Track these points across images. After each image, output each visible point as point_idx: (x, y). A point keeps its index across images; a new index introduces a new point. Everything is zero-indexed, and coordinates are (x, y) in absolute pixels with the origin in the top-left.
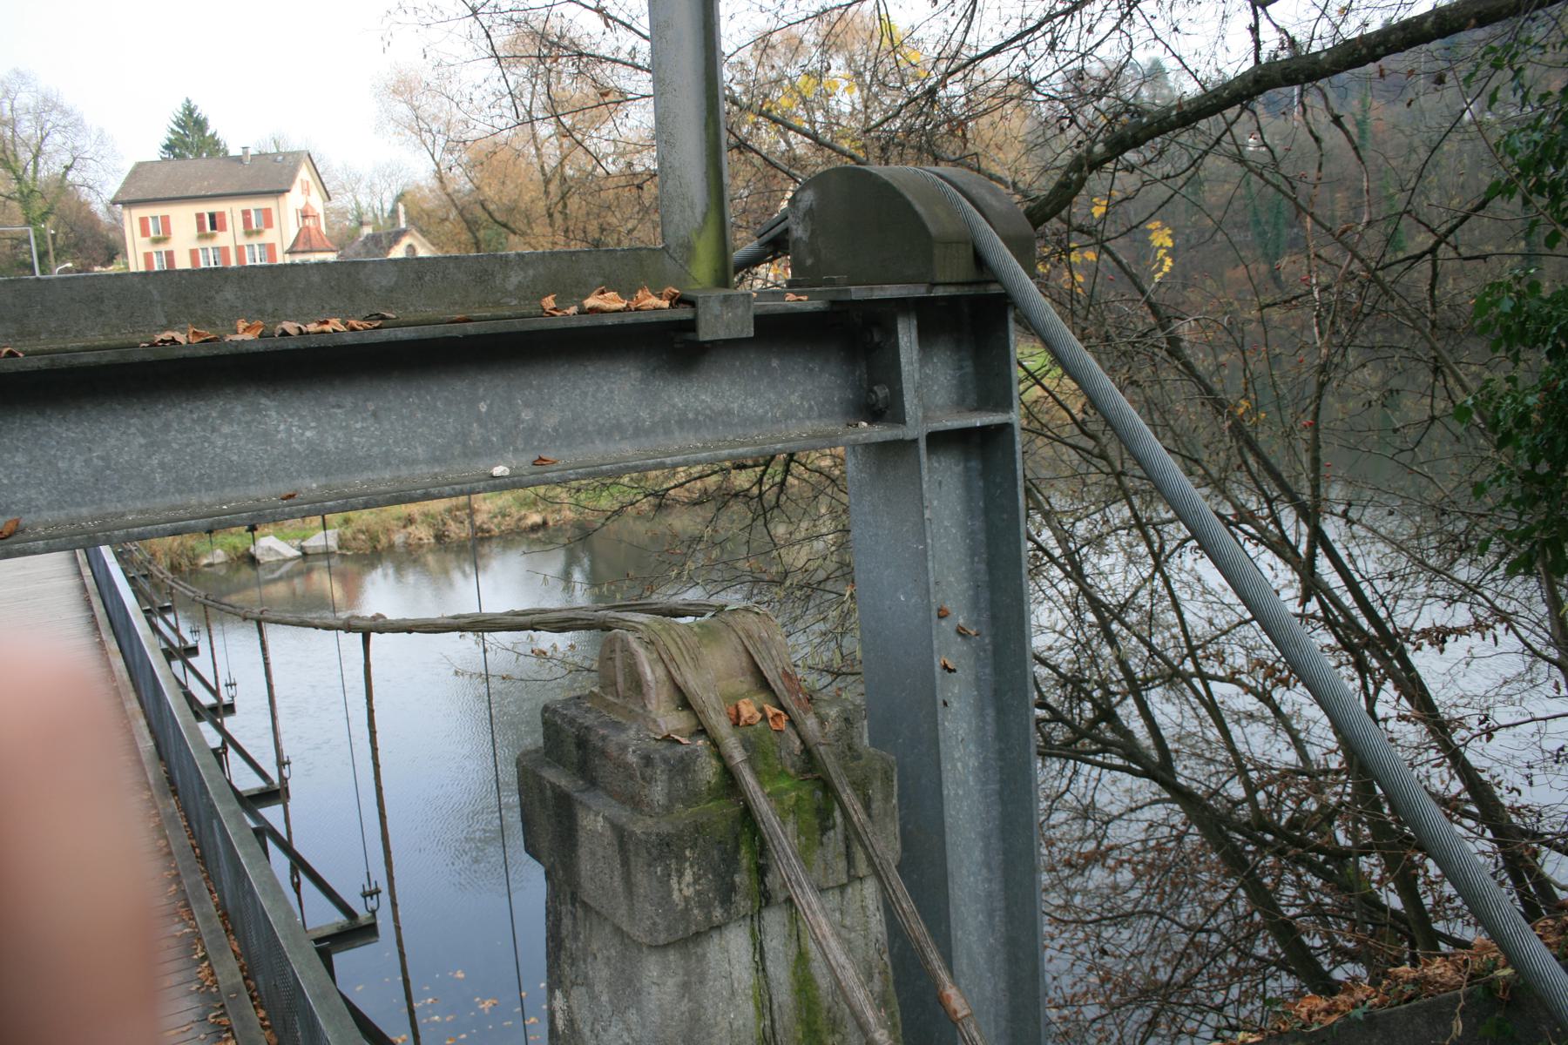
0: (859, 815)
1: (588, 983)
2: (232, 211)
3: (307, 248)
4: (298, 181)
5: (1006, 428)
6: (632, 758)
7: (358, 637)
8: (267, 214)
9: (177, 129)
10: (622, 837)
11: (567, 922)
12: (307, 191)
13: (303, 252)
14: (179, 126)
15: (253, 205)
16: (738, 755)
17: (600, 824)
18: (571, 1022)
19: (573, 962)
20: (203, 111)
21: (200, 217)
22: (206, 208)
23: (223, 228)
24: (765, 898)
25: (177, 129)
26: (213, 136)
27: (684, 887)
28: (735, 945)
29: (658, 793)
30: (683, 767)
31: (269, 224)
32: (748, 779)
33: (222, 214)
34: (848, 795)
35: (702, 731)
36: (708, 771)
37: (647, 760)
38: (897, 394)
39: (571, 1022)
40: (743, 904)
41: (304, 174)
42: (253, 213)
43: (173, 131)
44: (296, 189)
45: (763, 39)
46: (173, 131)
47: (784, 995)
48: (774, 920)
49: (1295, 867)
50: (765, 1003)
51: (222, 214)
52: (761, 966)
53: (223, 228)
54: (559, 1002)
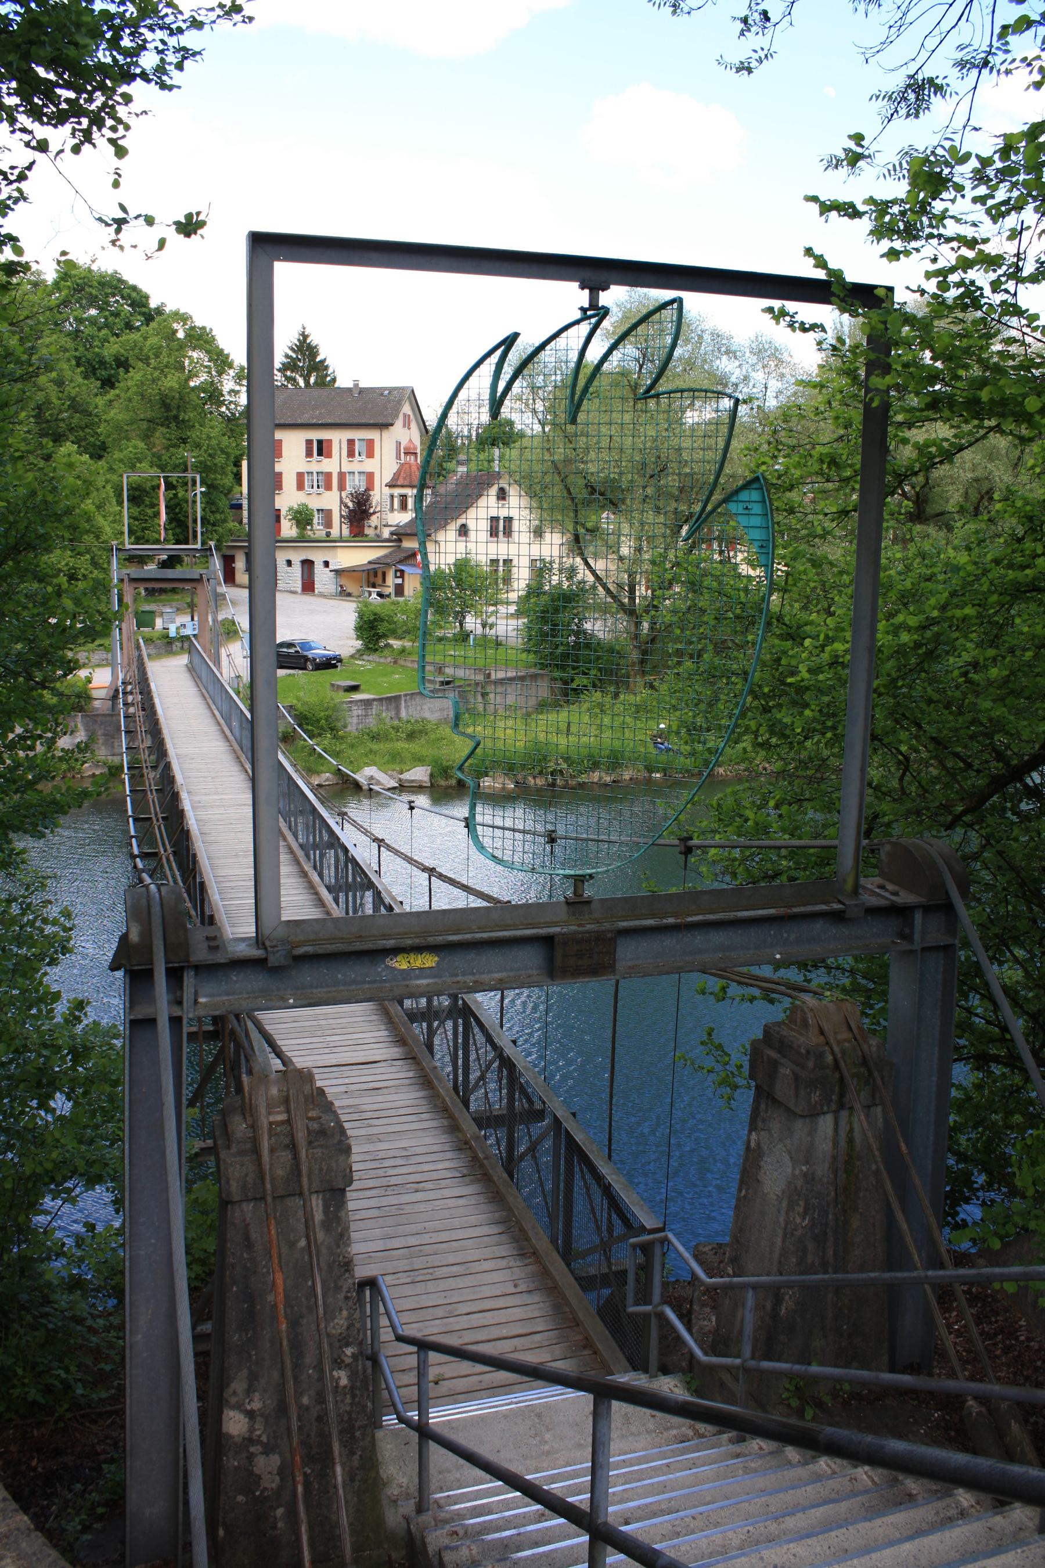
0: (879, 1082)
1: (769, 1130)
2: (338, 438)
3: (406, 483)
4: (401, 416)
5: (953, 945)
6: (803, 1051)
7: (426, 875)
8: (370, 443)
9: (291, 353)
10: (796, 1077)
11: (763, 1106)
12: (407, 424)
13: (402, 486)
14: (292, 349)
15: (357, 435)
16: (839, 1056)
17: (788, 1071)
18: (758, 1144)
19: (764, 1121)
20: (314, 339)
21: (309, 442)
22: (315, 435)
23: (329, 455)
24: (841, 1106)
25: (291, 353)
26: (323, 361)
27: (815, 1097)
28: (826, 1123)
29: (811, 1064)
30: (820, 1056)
31: (370, 454)
32: (842, 1064)
33: (330, 441)
34: (876, 1074)
35: (827, 1043)
36: (829, 1058)
37: (808, 1052)
38: (912, 933)
39: (758, 1144)
40: (834, 1107)
41: (406, 409)
42: (357, 443)
43: (287, 356)
44: (399, 423)
45: (874, 737)
46: (287, 356)
47: (843, 1143)
48: (844, 1114)
49: (60, 701)
50: (835, 1143)
51: (330, 441)
52: (836, 1130)
53: (329, 455)
54: (754, 1136)
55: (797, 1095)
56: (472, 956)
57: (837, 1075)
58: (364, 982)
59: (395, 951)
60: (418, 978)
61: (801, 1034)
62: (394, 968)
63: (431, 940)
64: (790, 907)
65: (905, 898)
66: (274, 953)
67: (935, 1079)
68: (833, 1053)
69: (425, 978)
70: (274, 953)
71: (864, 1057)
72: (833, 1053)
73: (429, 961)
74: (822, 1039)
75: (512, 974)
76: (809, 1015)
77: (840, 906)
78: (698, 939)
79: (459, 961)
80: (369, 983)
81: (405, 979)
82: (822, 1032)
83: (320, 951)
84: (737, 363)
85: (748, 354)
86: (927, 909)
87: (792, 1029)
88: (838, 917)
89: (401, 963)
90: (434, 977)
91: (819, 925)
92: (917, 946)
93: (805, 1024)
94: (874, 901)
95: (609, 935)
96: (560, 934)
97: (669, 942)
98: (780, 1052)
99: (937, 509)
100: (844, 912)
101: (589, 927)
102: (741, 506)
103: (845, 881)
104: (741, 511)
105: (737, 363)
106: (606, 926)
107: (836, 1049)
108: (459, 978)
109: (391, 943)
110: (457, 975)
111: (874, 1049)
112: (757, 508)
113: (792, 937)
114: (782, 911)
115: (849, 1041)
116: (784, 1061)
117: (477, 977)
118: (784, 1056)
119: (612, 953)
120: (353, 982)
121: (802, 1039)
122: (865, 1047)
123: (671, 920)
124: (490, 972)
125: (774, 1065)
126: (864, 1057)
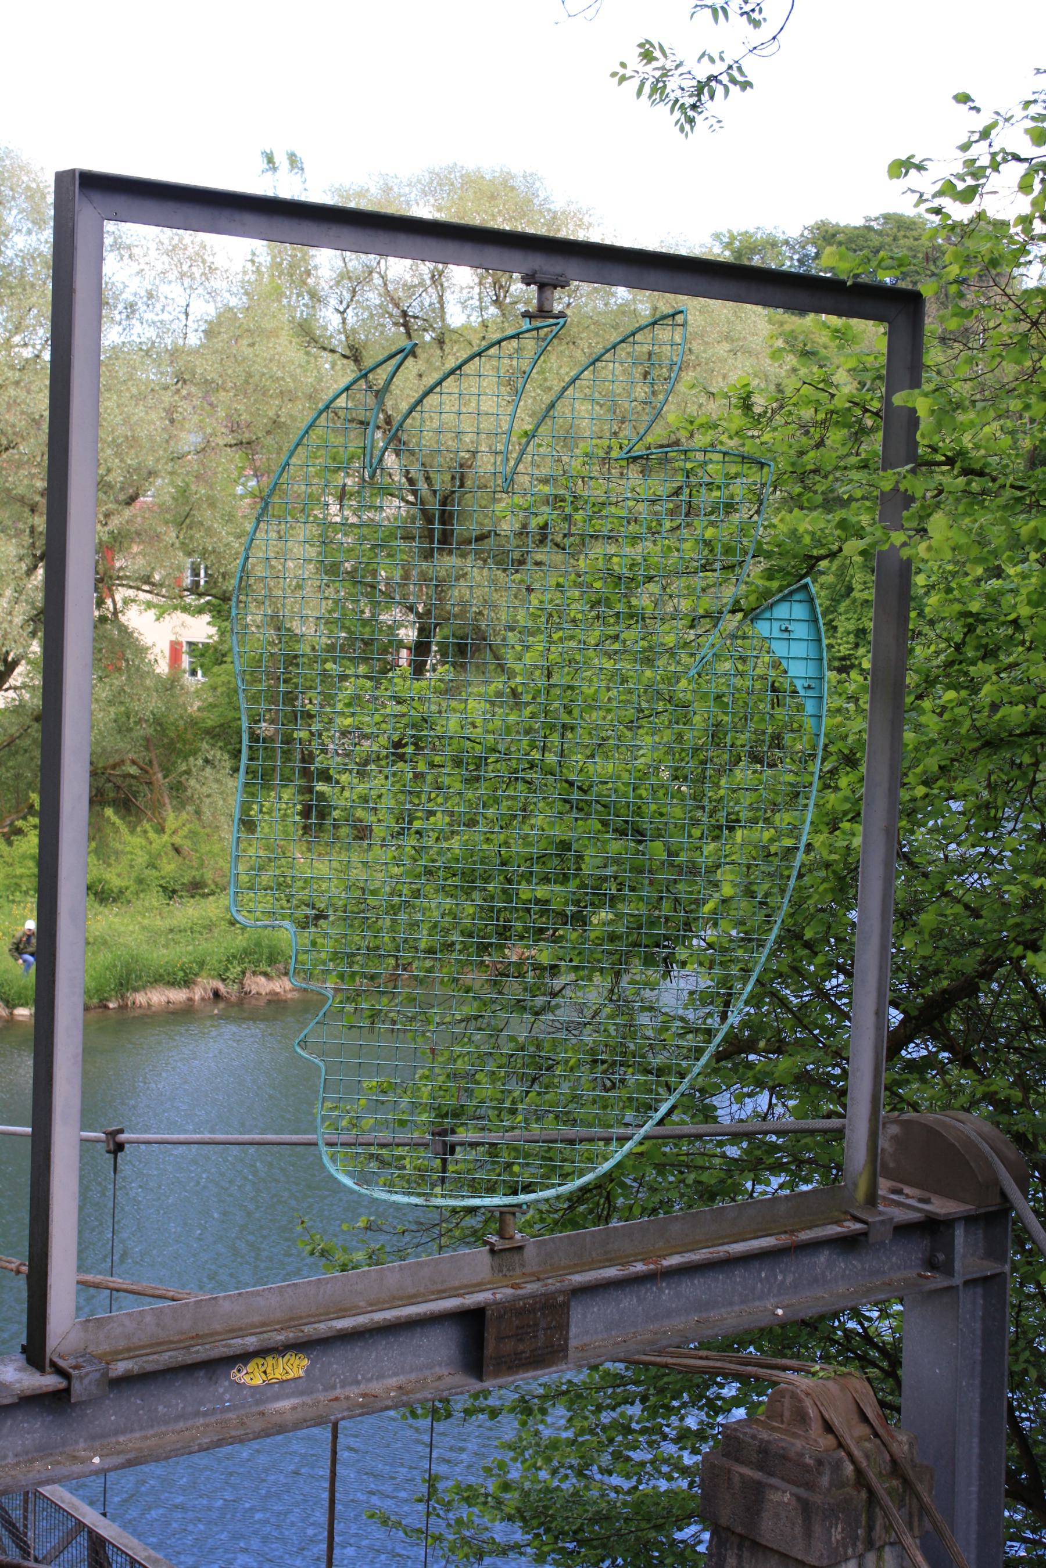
6: (808, 1460)
10: (806, 1508)
17: (787, 1497)
29: (825, 1481)
35: (840, 1445)
36: (849, 1469)
37: (820, 1462)
55: (808, 1534)
56: (356, 1351)
57: (864, 1495)
58: (197, 1414)
59: (244, 1358)
60: (277, 1398)
61: (794, 1435)
62: (242, 1386)
63: (310, 1330)
64: (792, 1232)
65: (941, 1207)
66: (81, 1378)
67: (974, 1489)
68: (853, 1461)
69: (288, 1396)
70: (81, 1378)
71: (894, 1461)
72: (853, 1461)
73: (294, 1366)
74: (829, 1441)
75: (413, 1377)
76: (808, 1403)
77: (859, 1226)
78: (666, 1294)
79: (337, 1361)
80: (205, 1414)
81: (258, 1402)
82: (828, 1428)
83: (150, 1368)
84: (135, 267)
85: (153, 254)
86: (970, 1220)
87: (773, 1429)
88: (849, 1244)
89: (252, 1376)
90: (301, 1393)
91: (823, 1258)
92: (958, 1281)
93: (801, 1417)
94: (901, 1215)
95: (560, 1299)
96: (496, 1303)
97: (628, 1301)
98: (760, 1468)
99: (473, 528)
100: (865, 1234)
101: (531, 1288)
102: (776, 625)
103: (855, 1185)
104: (776, 634)
105: (135, 267)
106: (553, 1284)
107: (857, 1453)
108: (338, 1392)
109: (251, 1342)
110: (334, 1387)
111: (906, 1447)
112: (801, 630)
113: (789, 1279)
114: (783, 1240)
115: (869, 1440)
116: (773, 1481)
117: (363, 1388)
118: (771, 1474)
119: (563, 1327)
120: (182, 1417)
121: (799, 1444)
122: (895, 1447)
123: (640, 1267)
124: (381, 1377)
125: (756, 1492)
126: (894, 1461)
